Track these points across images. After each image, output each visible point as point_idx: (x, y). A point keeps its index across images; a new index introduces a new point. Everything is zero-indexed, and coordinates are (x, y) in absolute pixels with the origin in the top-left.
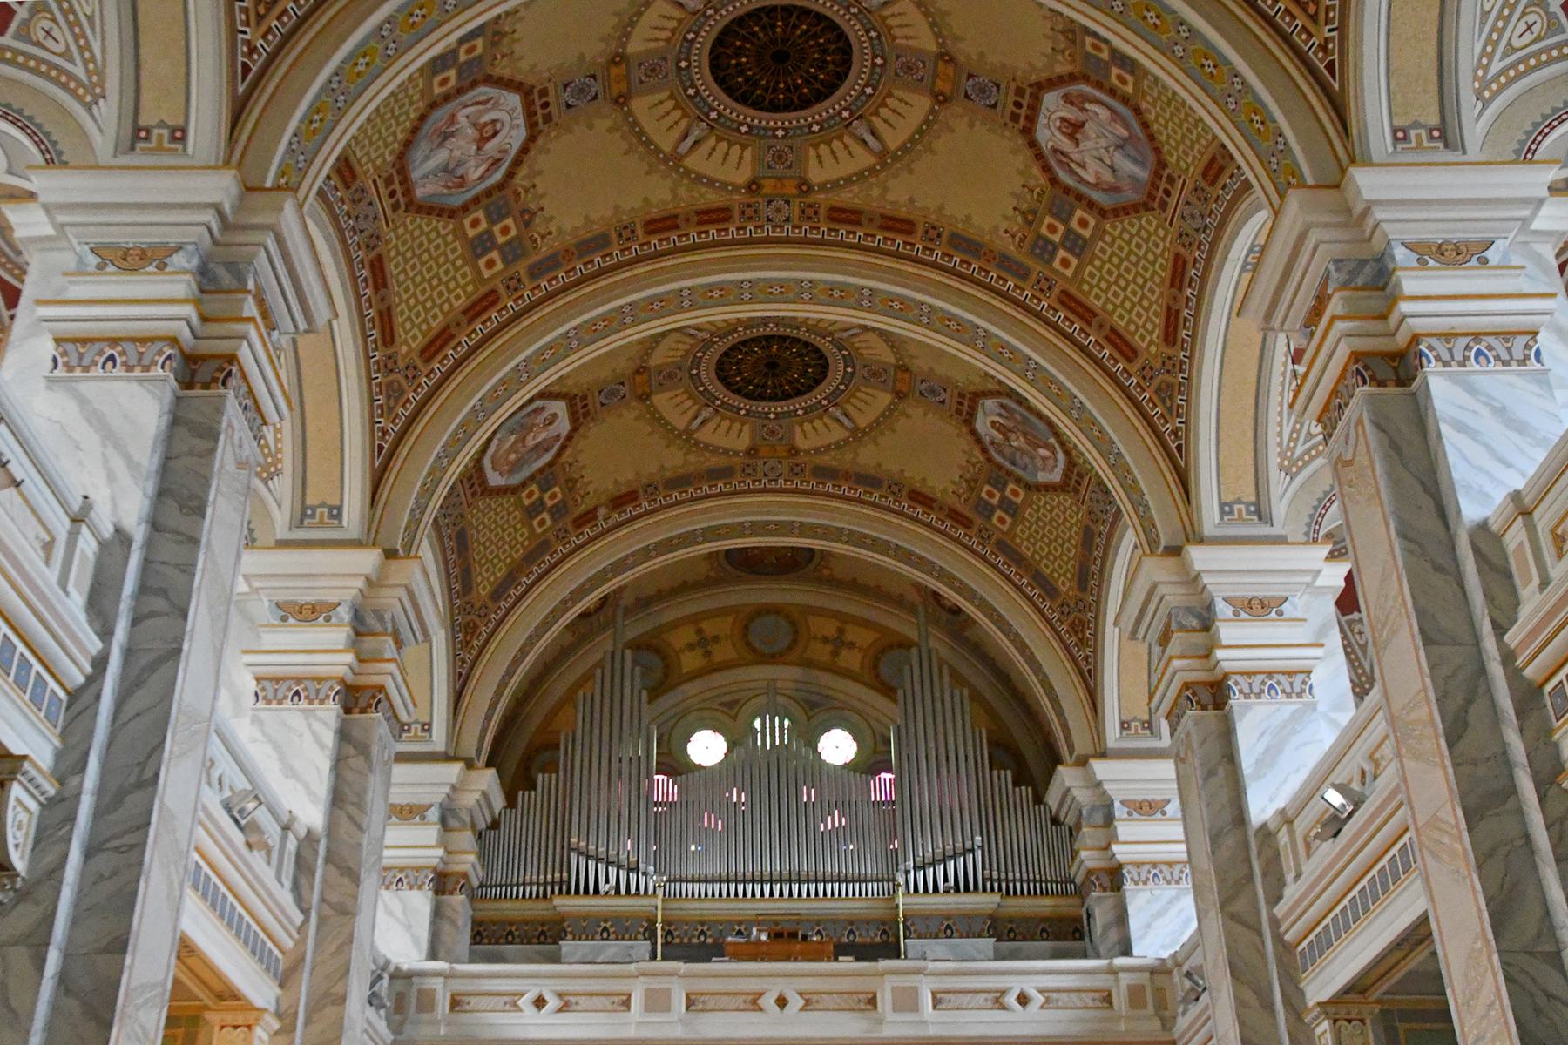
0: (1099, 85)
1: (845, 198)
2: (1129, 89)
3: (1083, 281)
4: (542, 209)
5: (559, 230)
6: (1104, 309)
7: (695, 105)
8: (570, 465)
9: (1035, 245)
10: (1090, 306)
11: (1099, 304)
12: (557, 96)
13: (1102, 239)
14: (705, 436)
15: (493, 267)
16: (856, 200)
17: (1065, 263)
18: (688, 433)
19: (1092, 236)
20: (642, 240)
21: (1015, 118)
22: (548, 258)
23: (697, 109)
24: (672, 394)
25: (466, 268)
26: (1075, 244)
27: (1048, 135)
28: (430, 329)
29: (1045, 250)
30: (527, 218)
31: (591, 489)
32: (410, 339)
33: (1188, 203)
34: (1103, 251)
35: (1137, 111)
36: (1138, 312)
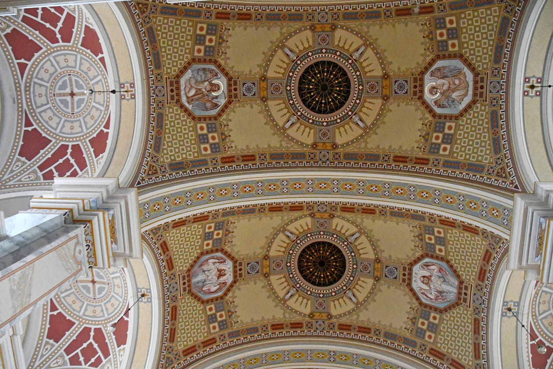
0: (432, 257)
1: (344, 320)
2: (443, 254)
3: (437, 343)
4: (230, 136)
5: (241, 321)
6: (447, 352)
7: (292, 281)
8: (231, 303)
9: (417, 331)
10: (442, 352)
11: (445, 350)
12: (245, 268)
13: (443, 323)
14: (291, 132)
15: (215, 329)
16: (355, 150)
17: (430, 337)
18: (283, 47)
19: (444, 235)
20: (268, 161)
21: (404, 280)
22: (236, 332)
23: (291, 280)
24: (279, 276)
25: (201, 230)
26: (433, 328)
27: (417, 284)
28: (187, 345)
29: (421, 333)
30: (230, 314)
31: (239, 320)
32: (180, 346)
33: (475, 294)
34: (444, 327)
35: (448, 262)
36: (483, 150)
